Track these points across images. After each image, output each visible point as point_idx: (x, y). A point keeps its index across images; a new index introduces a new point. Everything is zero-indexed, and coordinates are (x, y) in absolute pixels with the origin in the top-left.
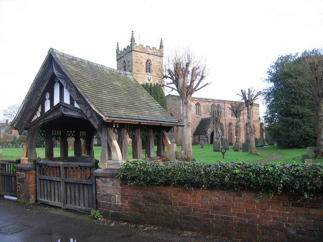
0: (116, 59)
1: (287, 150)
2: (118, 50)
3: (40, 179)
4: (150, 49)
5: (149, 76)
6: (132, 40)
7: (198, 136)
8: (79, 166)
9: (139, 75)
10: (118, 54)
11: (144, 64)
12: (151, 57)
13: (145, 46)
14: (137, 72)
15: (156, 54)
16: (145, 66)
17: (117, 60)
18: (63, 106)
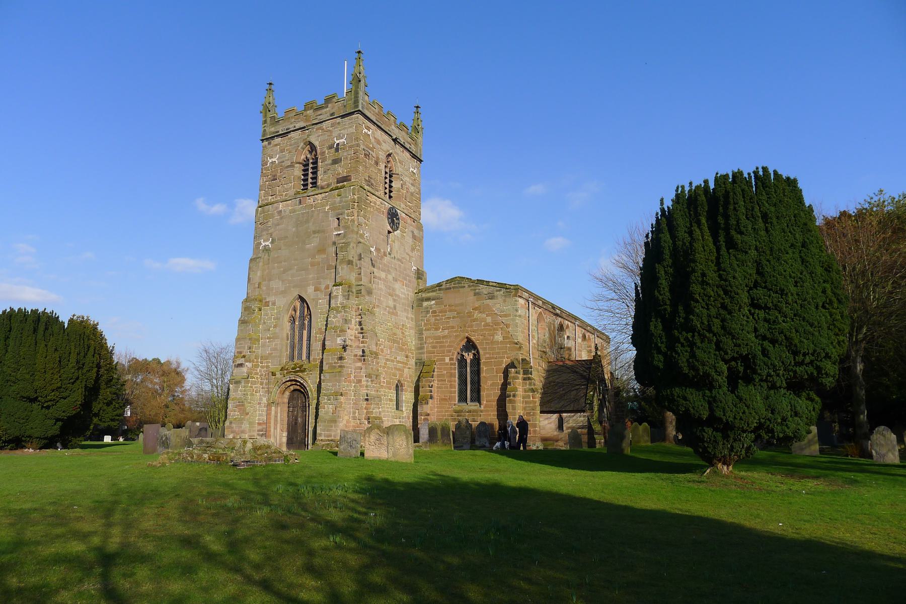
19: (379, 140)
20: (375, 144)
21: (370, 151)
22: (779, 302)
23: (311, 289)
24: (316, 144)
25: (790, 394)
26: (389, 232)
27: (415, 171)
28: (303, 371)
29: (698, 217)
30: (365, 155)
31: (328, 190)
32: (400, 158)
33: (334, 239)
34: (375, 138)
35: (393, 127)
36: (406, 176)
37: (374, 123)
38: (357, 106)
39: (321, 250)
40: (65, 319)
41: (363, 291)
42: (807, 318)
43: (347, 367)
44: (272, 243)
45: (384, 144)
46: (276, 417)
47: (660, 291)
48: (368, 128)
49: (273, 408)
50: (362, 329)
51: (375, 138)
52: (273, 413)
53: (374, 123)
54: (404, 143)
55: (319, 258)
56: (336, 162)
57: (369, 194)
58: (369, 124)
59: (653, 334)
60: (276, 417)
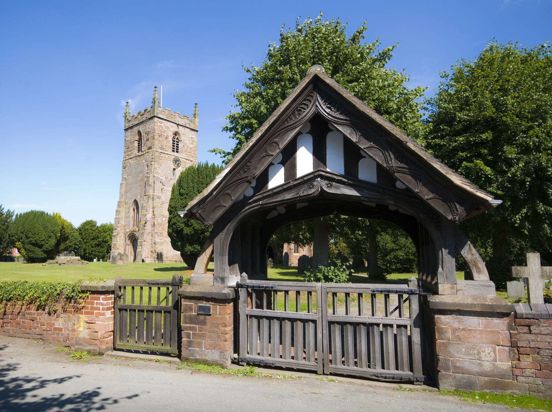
19: (168, 127)
21: (162, 133)
22: (532, 262)
23: (139, 197)
26: (174, 169)
27: (193, 137)
29: (465, 158)
30: (159, 136)
34: (165, 126)
35: (178, 118)
36: (187, 140)
37: (165, 120)
38: (154, 114)
40: (98, 224)
42: (416, 392)
43: (147, 230)
45: (172, 128)
46: (128, 250)
48: (161, 123)
49: (127, 247)
50: (154, 214)
51: (165, 126)
52: (127, 249)
53: (165, 120)
54: (186, 125)
57: (161, 153)
60: (128, 250)
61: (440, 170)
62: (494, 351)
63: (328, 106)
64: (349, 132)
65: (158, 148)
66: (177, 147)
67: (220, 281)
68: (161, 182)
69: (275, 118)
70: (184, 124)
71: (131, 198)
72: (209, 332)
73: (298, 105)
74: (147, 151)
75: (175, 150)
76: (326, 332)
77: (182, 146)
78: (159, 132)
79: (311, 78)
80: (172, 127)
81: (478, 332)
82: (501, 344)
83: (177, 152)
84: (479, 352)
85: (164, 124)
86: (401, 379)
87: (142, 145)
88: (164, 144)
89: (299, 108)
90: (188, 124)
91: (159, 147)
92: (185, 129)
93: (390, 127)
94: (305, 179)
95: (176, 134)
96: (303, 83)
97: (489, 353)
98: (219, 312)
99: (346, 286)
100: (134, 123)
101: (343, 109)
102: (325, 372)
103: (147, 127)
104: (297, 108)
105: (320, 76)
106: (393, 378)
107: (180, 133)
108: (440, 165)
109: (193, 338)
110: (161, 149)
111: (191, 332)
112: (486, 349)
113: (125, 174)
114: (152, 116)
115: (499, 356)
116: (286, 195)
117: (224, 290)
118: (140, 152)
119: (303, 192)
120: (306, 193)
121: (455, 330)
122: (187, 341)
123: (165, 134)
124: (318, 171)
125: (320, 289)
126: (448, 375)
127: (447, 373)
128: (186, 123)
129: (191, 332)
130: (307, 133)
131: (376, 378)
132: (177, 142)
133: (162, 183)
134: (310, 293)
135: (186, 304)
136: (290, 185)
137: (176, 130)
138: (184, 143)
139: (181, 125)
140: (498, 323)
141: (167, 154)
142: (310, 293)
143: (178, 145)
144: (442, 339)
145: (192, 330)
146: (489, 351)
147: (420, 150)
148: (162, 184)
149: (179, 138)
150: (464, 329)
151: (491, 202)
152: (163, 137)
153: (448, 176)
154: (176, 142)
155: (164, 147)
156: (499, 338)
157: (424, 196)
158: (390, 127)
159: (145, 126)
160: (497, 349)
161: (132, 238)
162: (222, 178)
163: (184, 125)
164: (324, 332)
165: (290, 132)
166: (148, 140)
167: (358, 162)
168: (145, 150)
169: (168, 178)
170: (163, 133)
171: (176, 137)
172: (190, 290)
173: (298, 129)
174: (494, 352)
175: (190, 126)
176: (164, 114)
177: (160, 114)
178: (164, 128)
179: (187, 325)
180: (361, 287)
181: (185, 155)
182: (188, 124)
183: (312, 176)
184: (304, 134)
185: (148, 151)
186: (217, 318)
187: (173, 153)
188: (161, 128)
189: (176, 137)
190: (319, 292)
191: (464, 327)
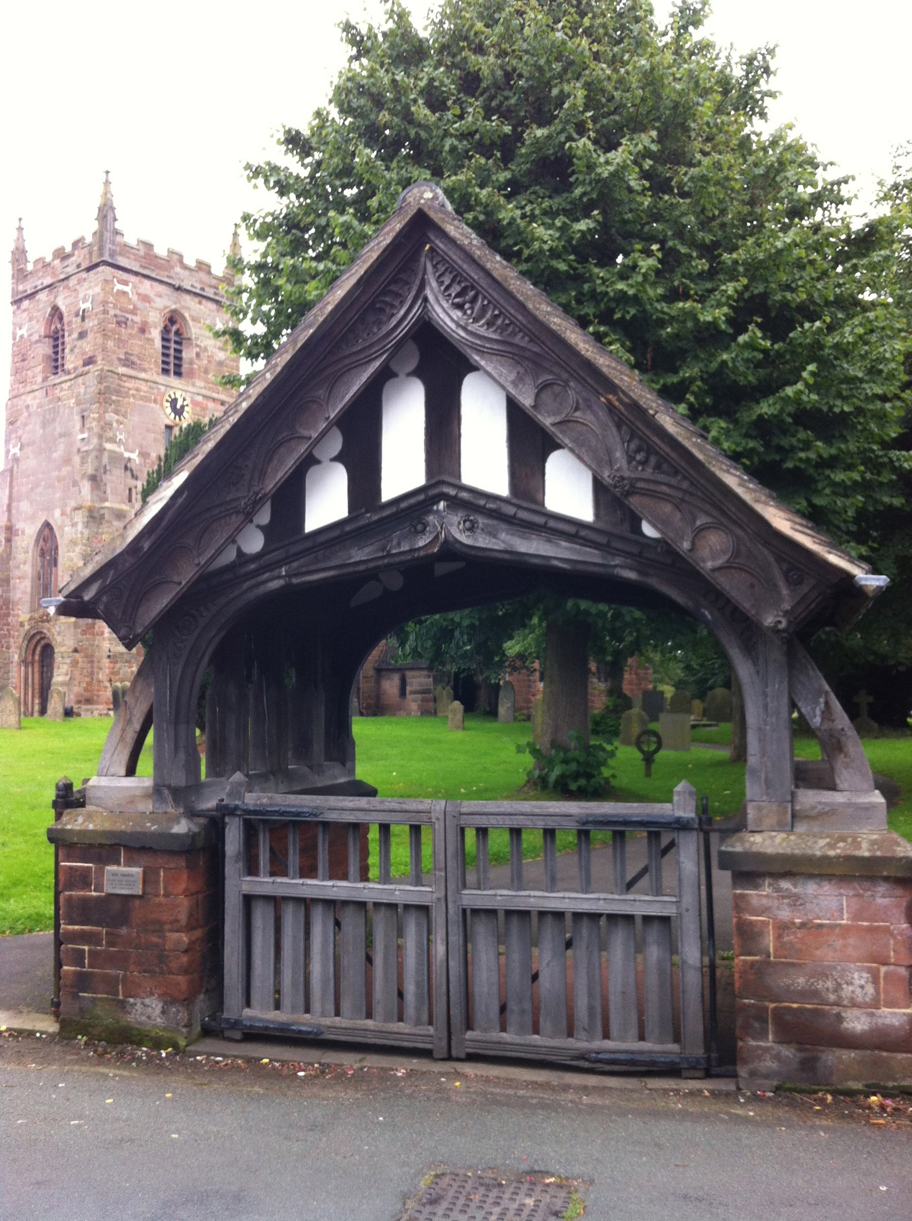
0: (10, 300)
1: (879, 742)
2: (19, 255)
3: (248, 900)
4: (186, 267)
5: (179, 389)
6: (106, 213)
7: (396, 679)
8: (603, 822)
9: (130, 384)
10: (20, 274)
11: (156, 334)
12: (190, 307)
13: (161, 250)
14: (122, 370)
15: (209, 293)
16: (158, 343)
17: (17, 302)
18: (455, 503)
20: (140, 304)
23: (57, 513)
24: (63, 308)
25: (178, 1011)
28: (48, 621)
31: (73, 376)
32: (194, 313)
33: (79, 445)
34: (138, 294)
37: (137, 274)
39: (67, 461)
41: (107, 516)
44: (21, 449)
45: (158, 300)
47: (88, 683)
48: (125, 283)
53: (137, 274)
54: (203, 289)
55: (65, 471)
56: (82, 335)
58: (125, 276)
59: (745, 449)
61: (739, 491)
62: (875, 980)
63: (457, 300)
64: (513, 376)
65: (116, 362)
66: (175, 358)
67: (170, 798)
68: (126, 468)
69: (311, 331)
70: (199, 286)
71: (33, 518)
72: (137, 947)
73: (377, 296)
74: (81, 370)
75: (172, 367)
76: (456, 938)
77: (194, 355)
78: (118, 312)
79: (407, 220)
80: (160, 296)
81: (837, 931)
82: (892, 960)
83: (178, 374)
84: (839, 985)
85: (134, 287)
86: (653, 1063)
87: (67, 351)
88: (136, 350)
89: (378, 306)
90: (211, 286)
91: (119, 359)
92: (200, 303)
93: (614, 369)
94: (404, 505)
95: (173, 319)
96: (388, 233)
97: (862, 987)
98: (165, 888)
99: (509, 810)
100: (39, 283)
101: (497, 312)
102: (454, 1053)
103: (81, 296)
104: (373, 303)
105: (432, 214)
106: (633, 1062)
107: (187, 315)
108: (738, 477)
109: (90, 966)
110: (125, 365)
111: (86, 948)
112: (856, 975)
113: (13, 442)
114: (95, 260)
115: (886, 992)
116: (353, 552)
117: (178, 823)
118: (60, 373)
119: (399, 544)
120: (405, 547)
121: (783, 927)
122: (75, 973)
123: (137, 319)
124: (443, 482)
125: (442, 817)
126: (760, 1047)
127: (761, 1044)
128: (201, 282)
129: (86, 948)
130: (410, 374)
131: (586, 1064)
132: (176, 342)
133: (132, 471)
134: (416, 830)
135: (71, 868)
136: (362, 522)
137: (174, 307)
138: (197, 346)
139: (188, 292)
140: (886, 907)
141: (147, 381)
142: (416, 830)
143: (180, 351)
144: (749, 954)
145: (88, 943)
146: (862, 982)
147: (688, 435)
148: (129, 473)
149: (183, 330)
150: (803, 925)
151: (863, 583)
152: (132, 327)
153: (759, 508)
154: (173, 346)
155: (135, 359)
156: (887, 946)
157: (704, 561)
158: (614, 369)
159: (74, 294)
160: (882, 975)
161: (39, 642)
162: (164, 502)
163: (198, 291)
164: (452, 939)
165: (355, 371)
166: (82, 335)
167: (544, 460)
168: (75, 369)
169: (149, 455)
170: (130, 316)
171: (174, 328)
172: (82, 828)
173: (377, 364)
174: (873, 983)
175: (215, 294)
176: (135, 255)
177: (121, 254)
178: (135, 298)
179: (76, 927)
180: (551, 810)
181: (202, 384)
182: (211, 286)
183: (422, 497)
184: (402, 376)
185: (87, 368)
186: (159, 905)
187: (162, 379)
188: (123, 299)
189: (174, 328)
190: (439, 826)
191: (805, 919)
